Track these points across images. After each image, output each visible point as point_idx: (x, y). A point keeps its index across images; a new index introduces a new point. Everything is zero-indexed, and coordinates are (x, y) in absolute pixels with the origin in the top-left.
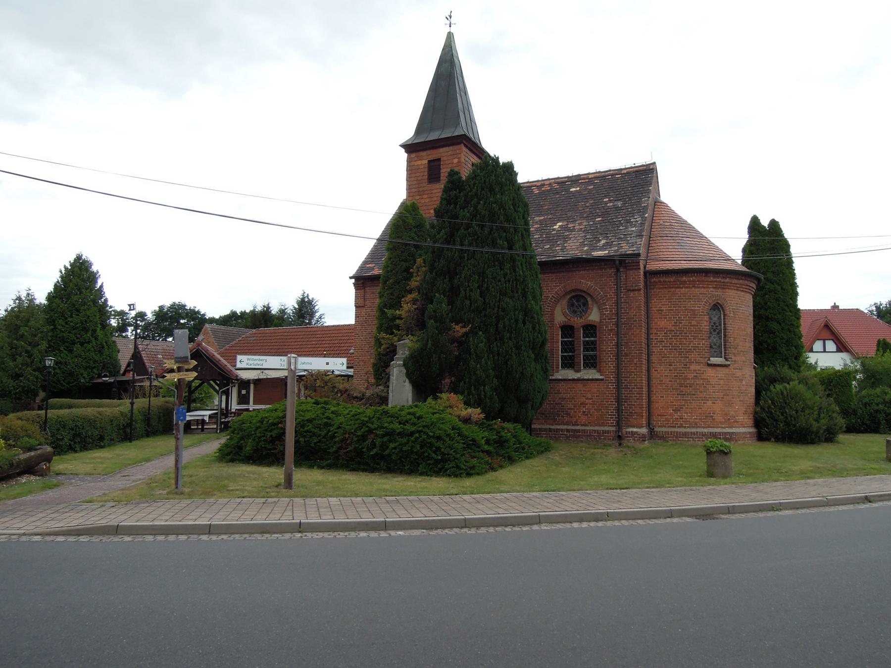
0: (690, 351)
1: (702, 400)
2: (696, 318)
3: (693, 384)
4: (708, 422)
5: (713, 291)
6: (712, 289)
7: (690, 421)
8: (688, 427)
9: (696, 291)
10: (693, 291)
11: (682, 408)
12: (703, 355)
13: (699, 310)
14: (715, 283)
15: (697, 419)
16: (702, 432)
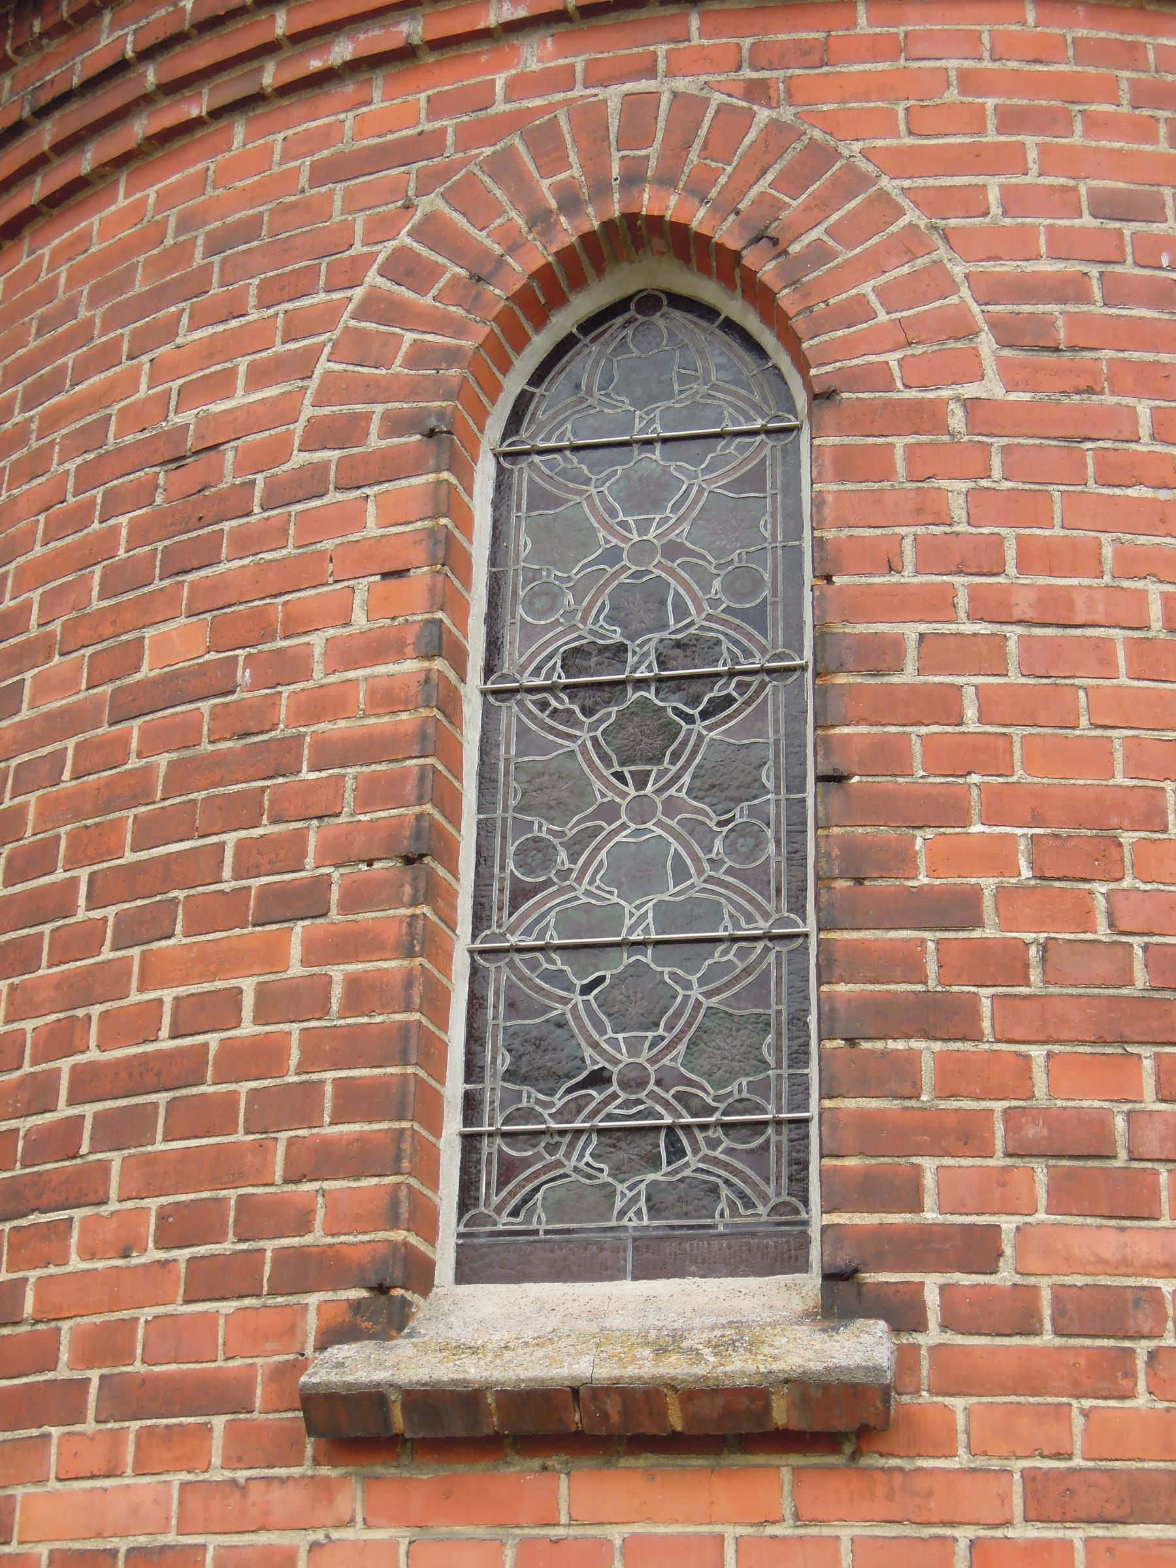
13: (284, 411)
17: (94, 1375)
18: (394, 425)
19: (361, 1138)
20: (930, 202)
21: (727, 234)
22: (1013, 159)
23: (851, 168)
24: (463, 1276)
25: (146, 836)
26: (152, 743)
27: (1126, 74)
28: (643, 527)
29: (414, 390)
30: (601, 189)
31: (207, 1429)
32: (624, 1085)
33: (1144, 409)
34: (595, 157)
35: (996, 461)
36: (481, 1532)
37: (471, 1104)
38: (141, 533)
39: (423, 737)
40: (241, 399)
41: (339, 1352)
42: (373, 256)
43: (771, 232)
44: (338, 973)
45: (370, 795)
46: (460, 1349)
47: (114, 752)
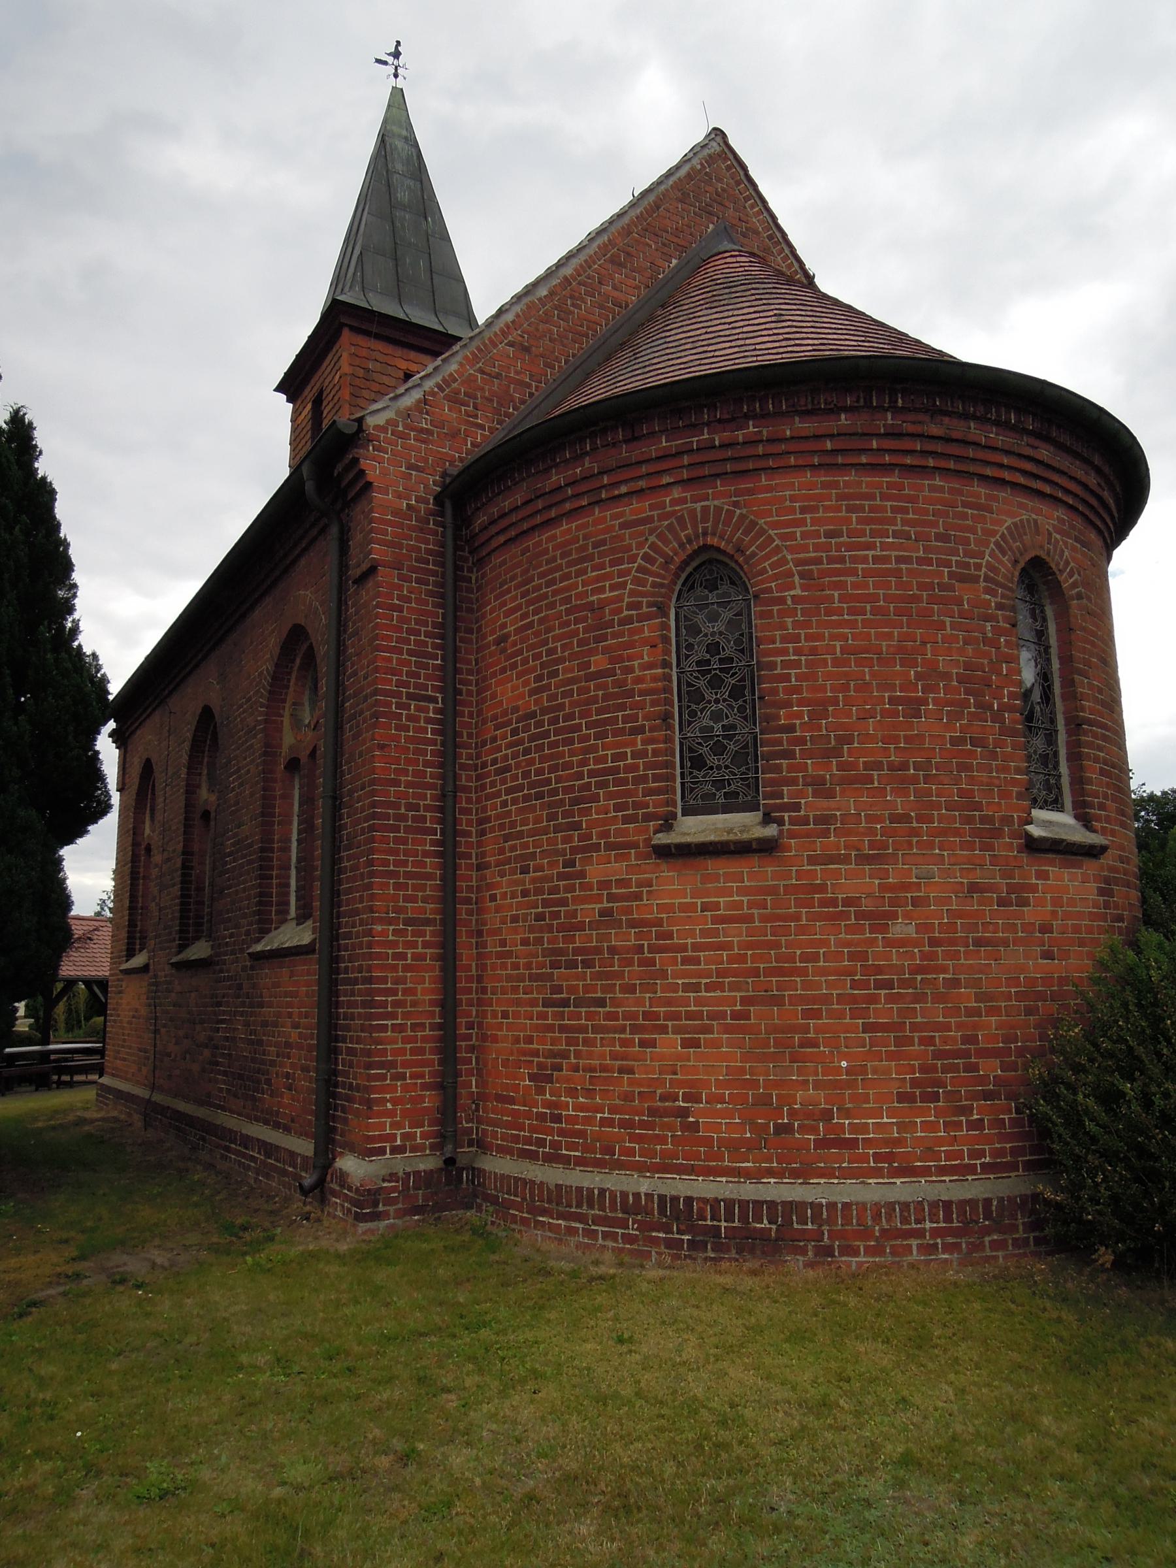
0: (584, 798)
1: (635, 1029)
2: (604, 638)
3: (598, 950)
4: (662, 1140)
5: (683, 501)
7: (582, 1134)
8: (580, 1162)
9: (607, 518)
10: (596, 523)
12: (637, 806)
13: (619, 599)
14: (686, 460)
16: (624, 1195)
17: (602, 841)
18: (650, 605)
19: (659, 786)
20: (783, 537)
21: (730, 549)
22: (802, 522)
23: (761, 527)
24: (683, 815)
25: (599, 711)
26: (597, 688)
27: (834, 491)
28: (713, 627)
29: (653, 595)
30: (697, 537)
31: (630, 853)
32: (717, 769)
33: (836, 594)
34: (695, 527)
35: (799, 612)
36: (692, 872)
37: (682, 774)
38: (585, 630)
39: (664, 689)
40: (608, 594)
41: (660, 835)
42: (639, 554)
44: (650, 747)
46: (685, 834)
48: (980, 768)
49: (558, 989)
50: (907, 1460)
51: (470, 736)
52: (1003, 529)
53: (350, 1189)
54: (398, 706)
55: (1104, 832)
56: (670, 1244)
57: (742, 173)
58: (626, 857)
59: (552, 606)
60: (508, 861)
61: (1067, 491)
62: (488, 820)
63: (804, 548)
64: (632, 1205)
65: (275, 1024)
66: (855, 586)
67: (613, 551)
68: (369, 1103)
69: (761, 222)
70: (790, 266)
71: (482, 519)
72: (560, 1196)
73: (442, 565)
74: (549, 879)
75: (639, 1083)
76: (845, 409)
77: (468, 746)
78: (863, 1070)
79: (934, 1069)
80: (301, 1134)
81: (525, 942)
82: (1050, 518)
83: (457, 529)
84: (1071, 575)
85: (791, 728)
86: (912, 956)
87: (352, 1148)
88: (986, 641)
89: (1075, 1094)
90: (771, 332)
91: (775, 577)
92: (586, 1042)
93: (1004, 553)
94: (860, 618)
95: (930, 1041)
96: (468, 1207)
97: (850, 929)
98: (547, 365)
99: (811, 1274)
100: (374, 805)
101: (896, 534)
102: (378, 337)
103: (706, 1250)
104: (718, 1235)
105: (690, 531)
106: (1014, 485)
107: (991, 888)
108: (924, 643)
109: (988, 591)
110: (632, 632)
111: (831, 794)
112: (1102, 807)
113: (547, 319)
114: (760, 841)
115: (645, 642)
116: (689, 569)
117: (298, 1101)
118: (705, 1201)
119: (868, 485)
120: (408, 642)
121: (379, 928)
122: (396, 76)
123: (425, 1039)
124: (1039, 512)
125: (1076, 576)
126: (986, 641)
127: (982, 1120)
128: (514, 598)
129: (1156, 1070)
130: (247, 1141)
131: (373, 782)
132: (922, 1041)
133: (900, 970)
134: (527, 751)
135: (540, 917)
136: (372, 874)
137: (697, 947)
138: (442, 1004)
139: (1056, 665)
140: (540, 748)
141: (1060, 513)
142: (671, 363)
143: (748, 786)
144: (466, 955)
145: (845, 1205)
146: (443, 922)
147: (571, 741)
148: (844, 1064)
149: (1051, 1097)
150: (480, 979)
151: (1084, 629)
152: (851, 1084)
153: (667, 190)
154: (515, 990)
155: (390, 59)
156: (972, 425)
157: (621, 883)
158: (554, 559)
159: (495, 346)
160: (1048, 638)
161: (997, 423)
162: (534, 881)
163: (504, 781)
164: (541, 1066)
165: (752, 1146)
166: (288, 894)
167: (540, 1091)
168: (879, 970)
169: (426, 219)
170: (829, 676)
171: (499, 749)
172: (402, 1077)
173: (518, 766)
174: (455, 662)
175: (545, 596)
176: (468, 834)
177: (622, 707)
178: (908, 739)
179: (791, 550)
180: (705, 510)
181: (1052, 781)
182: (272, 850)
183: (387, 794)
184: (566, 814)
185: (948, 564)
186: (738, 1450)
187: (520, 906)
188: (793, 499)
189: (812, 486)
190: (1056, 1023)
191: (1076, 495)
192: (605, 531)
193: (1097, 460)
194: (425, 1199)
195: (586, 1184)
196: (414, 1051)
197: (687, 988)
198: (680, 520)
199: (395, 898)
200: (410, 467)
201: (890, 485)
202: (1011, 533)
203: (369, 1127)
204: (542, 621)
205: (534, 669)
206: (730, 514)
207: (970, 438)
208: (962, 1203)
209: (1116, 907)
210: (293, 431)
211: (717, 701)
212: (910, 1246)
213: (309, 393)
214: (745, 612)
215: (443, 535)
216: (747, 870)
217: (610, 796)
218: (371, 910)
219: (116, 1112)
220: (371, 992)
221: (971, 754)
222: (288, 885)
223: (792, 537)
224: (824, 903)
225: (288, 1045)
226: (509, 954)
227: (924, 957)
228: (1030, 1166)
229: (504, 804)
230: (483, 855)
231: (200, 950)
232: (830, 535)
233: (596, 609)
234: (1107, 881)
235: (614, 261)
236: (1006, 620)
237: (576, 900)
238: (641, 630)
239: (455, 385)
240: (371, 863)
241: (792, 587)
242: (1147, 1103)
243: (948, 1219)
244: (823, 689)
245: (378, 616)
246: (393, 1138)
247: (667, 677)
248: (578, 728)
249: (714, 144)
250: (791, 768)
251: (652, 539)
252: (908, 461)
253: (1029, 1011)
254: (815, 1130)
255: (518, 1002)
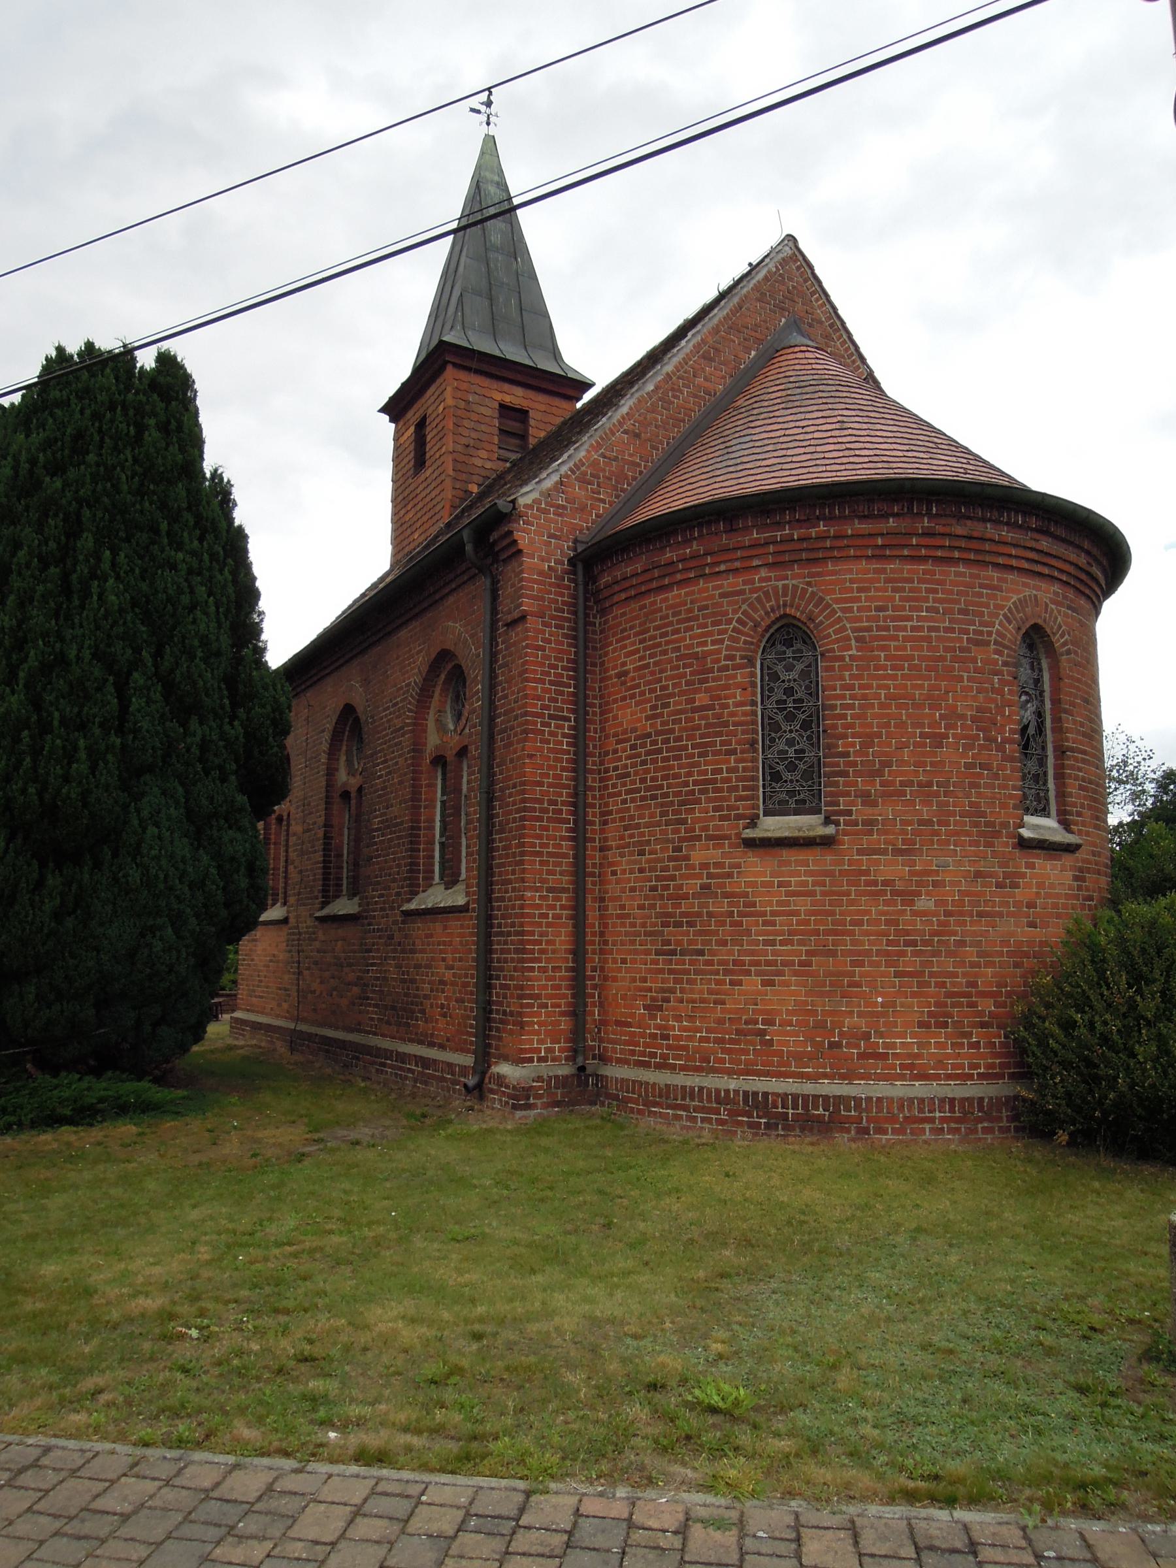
0: (690, 801)
1: (727, 972)
2: (706, 681)
3: (699, 915)
4: (746, 1052)
5: (769, 579)
6: (764, 573)
7: (685, 1048)
8: (683, 1068)
9: (708, 589)
10: (700, 591)
11: (667, 1000)
13: (719, 652)
14: (771, 549)
15: (707, 1040)
16: (718, 1091)
18: (742, 658)
20: (844, 610)
21: (803, 618)
22: (858, 599)
30: (779, 607)
34: (777, 600)
37: (764, 786)
38: (692, 674)
40: (710, 647)
41: (747, 831)
43: (492, 119)
45: (743, 732)
47: (693, 719)
48: (987, 786)
49: (668, 943)
50: (919, 1230)
51: (595, 747)
52: (1010, 604)
53: (507, 1087)
54: (543, 724)
55: (1080, 833)
56: (751, 1125)
57: (809, 271)
58: (722, 846)
59: (665, 652)
60: (628, 845)
61: (1061, 571)
62: (610, 813)
63: (859, 620)
64: (723, 1098)
65: (428, 966)
66: (897, 648)
67: (714, 614)
68: (522, 1025)
69: (824, 313)
70: (848, 349)
71: (606, 579)
72: (668, 1092)
73: (575, 613)
74: (661, 860)
75: (730, 1011)
76: (894, 515)
77: (593, 755)
78: (894, 1005)
79: (945, 1005)
80: (463, 1050)
81: (641, 907)
82: (1047, 592)
83: (586, 585)
84: (1062, 636)
85: (846, 754)
86: (931, 923)
87: (506, 1058)
88: (993, 690)
89: (1044, 1022)
90: (835, 440)
91: (837, 641)
92: (689, 981)
93: (1010, 622)
94: (899, 673)
95: (943, 985)
96: (594, 1103)
97: (886, 903)
98: (653, 447)
99: (854, 1146)
100: (524, 801)
101: (928, 610)
102: (478, 372)
103: (777, 1129)
104: (787, 1119)
105: (773, 603)
106: (1019, 569)
107: (991, 875)
108: (947, 692)
109: (997, 652)
110: (728, 677)
111: (874, 804)
112: (1079, 814)
113: (653, 410)
114: (823, 837)
115: (737, 686)
116: (772, 631)
117: (453, 1025)
118: (777, 1095)
119: (909, 571)
120: (548, 674)
121: (529, 894)
122: (488, 124)
123: (562, 979)
124: (1038, 589)
125: (1067, 636)
126: (993, 690)
127: (979, 1042)
128: (633, 644)
129: (1099, 1005)
130: (403, 1057)
131: (523, 783)
132: (937, 985)
133: (921, 933)
134: (644, 763)
135: (653, 889)
136: (523, 854)
137: (773, 913)
138: (574, 952)
139: (1048, 705)
140: (654, 761)
141: (1056, 588)
142: (759, 463)
143: (813, 795)
144: (592, 916)
145: (879, 1099)
146: (575, 891)
147: (679, 758)
148: (880, 1000)
149: (1029, 1026)
150: (602, 934)
151: (1069, 677)
152: (884, 1014)
153: (748, 292)
154: (633, 942)
155: (483, 108)
156: (988, 525)
157: (718, 865)
158: (667, 617)
159: (613, 434)
160: (1042, 685)
161: (1008, 524)
162: (648, 861)
163: (624, 785)
164: (653, 999)
165: (812, 1057)
166: (433, 865)
167: (654, 1017)
168: (907, 933)
169: (516, 259)
170: (875, 716)
171: (620, 759)
172: (545, 1006)
173: (636, 773)
174: (585, 690)
175: (659, 645)
176: (593, 823)
177: (720, 734)
178: (932, 764)
179: (850, 620)
180: (785, 587)
181: (1042, 794)
182: (419, 829)
183: (534, 792)
184: (675, 812)
185: (966, 632)
186: (813, 1224)
187: (636, 880)
188: (852, 581)
189: (867, 572)
190: (1034, 973)
191: (1069, 574)
192: (706, 599)
193: (1086, 545)
194: (563, 1095)
195: (688, 1084)
196: (554, 987)
197: (766, 943)
198: (766, 594)
199: (540, 872)
200: (550, 536)
201: (925, 572)
202: (1016, 607)
203: (522, 1042)
204: (656, 664)
205: (649, 700)
206: (804, 591)
207: (988, 536)
208: (963, 1100)
209: (1088, 890)
210: (396, 449)
211: (791, 731)
212: (924, 1129)
213: (413, 416)
214: (813, 664)
215: (576, 589)
216: (813, 859)
217: (709, 800)
218: (523, 880)
219: (260, 1040)
220: (522, 942)
221: (980, 776)
222: (433, 857)
223: (850, 610)
224: (868, 883)
225: (442, 982)
226: (628, 916)
227: (940, 923)
228: (1012, 1076)
229: (624, 802)
230: (606, 839)
231: (344, 906)
232: (878, 609)
233: (700, 658)
234: (1081, 870)
235: (706, 357)
236: (1009, 674)
237: (682, 877)
238: (735, 677)
239: (583, 468)
240: (523, 845)
241: (849, 648)
242: (1091, 1026)
243: (952, 1110)
244: (871, 725)
245: (526, 654)
246: (538, 1050)
247: (754, 713)
248: (685, 748)
249: (787, 248)
250: (846, 784)
251: (744, 607)
252: (939, 553)
253: (1017, 965)
254: (858, 1046)
255: (636, 952)
